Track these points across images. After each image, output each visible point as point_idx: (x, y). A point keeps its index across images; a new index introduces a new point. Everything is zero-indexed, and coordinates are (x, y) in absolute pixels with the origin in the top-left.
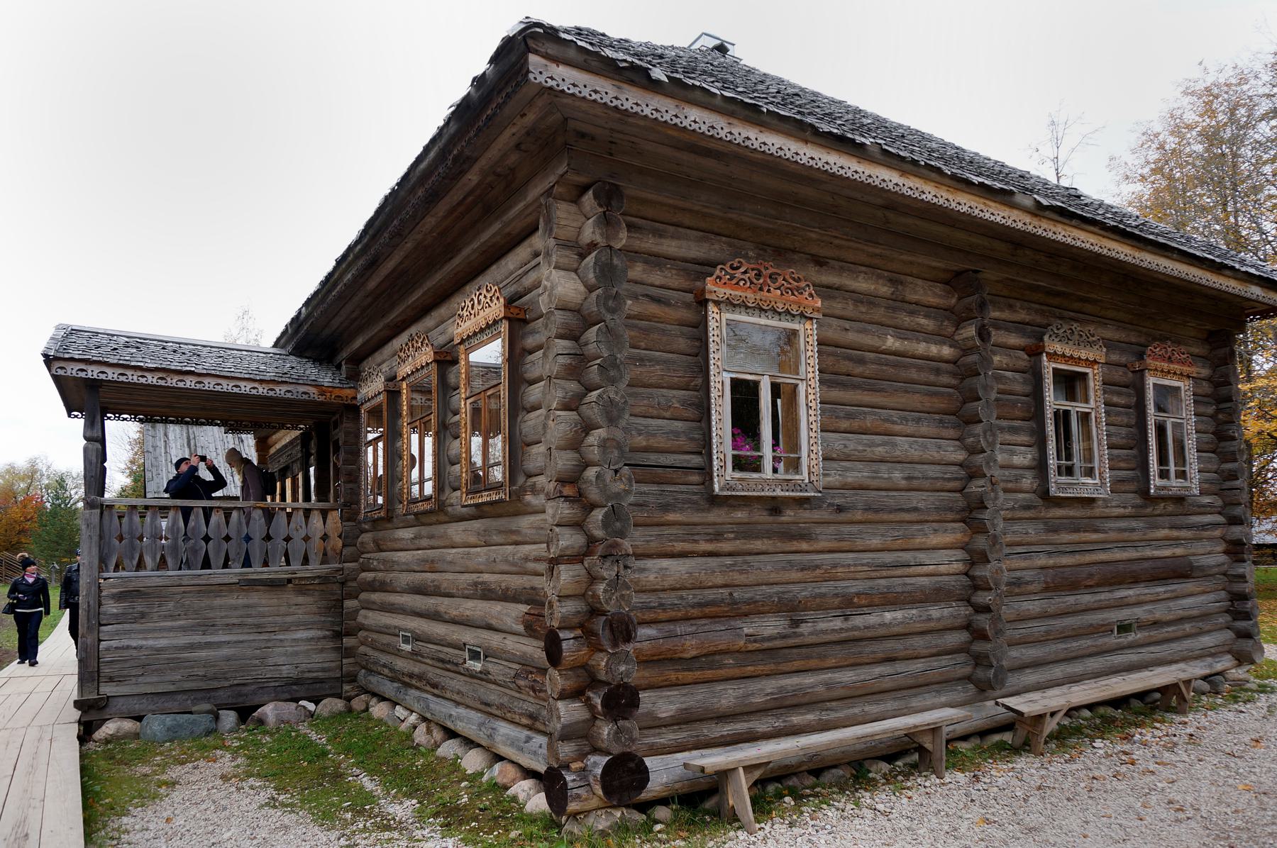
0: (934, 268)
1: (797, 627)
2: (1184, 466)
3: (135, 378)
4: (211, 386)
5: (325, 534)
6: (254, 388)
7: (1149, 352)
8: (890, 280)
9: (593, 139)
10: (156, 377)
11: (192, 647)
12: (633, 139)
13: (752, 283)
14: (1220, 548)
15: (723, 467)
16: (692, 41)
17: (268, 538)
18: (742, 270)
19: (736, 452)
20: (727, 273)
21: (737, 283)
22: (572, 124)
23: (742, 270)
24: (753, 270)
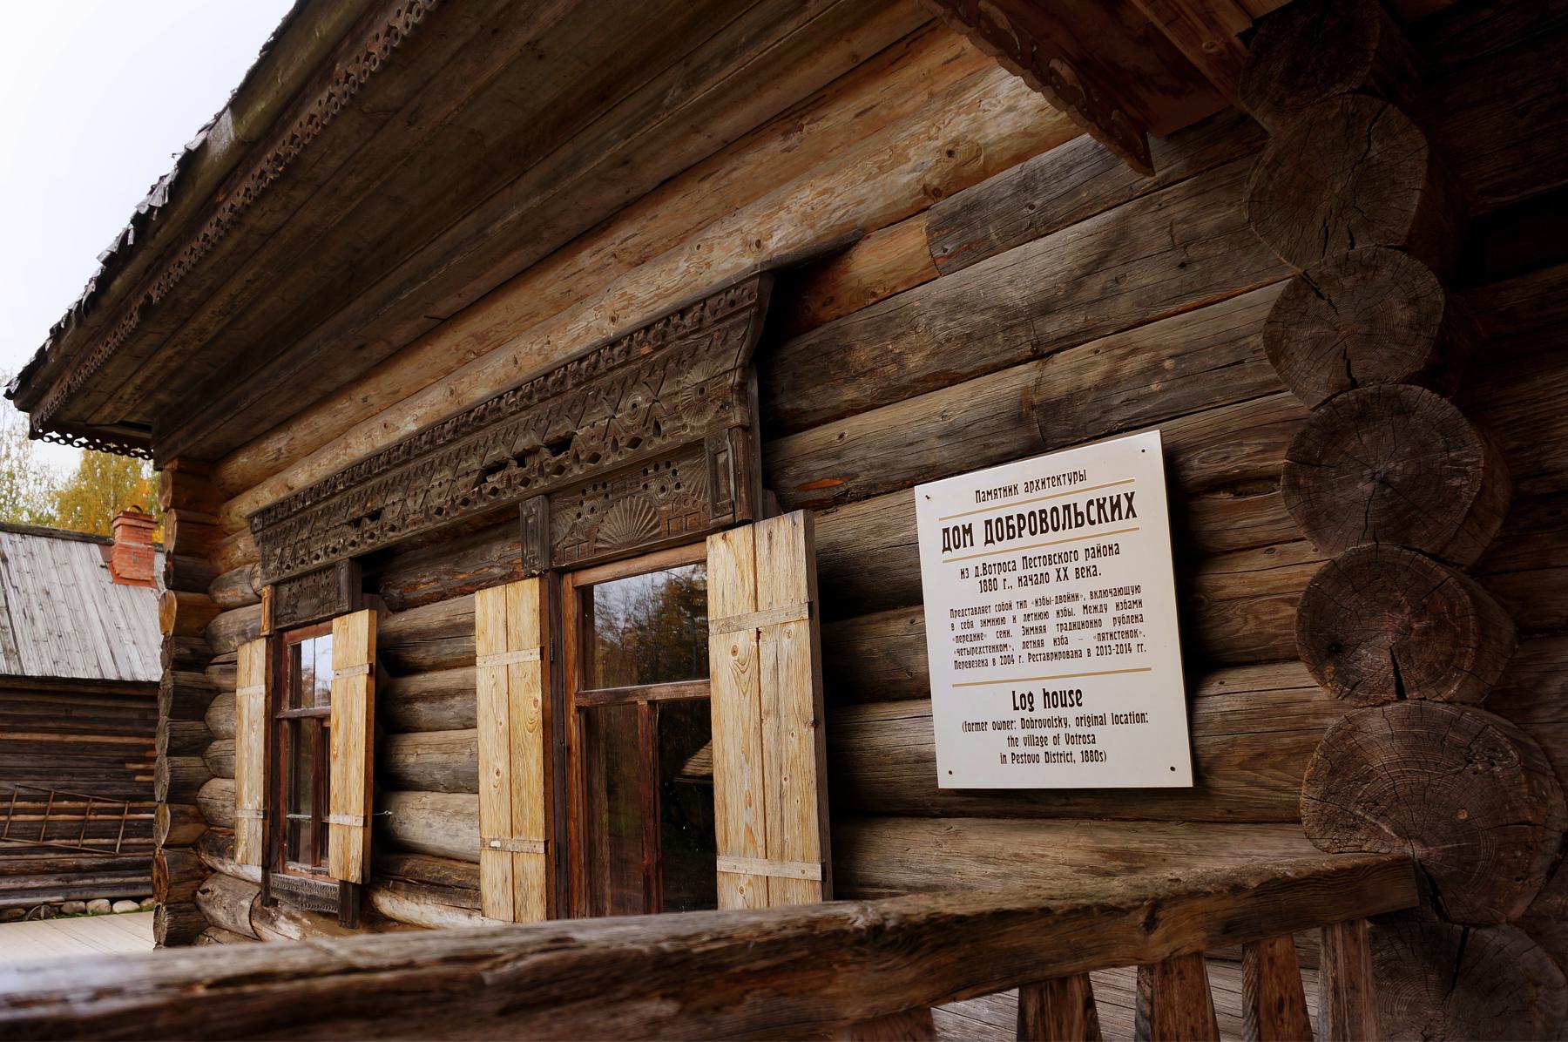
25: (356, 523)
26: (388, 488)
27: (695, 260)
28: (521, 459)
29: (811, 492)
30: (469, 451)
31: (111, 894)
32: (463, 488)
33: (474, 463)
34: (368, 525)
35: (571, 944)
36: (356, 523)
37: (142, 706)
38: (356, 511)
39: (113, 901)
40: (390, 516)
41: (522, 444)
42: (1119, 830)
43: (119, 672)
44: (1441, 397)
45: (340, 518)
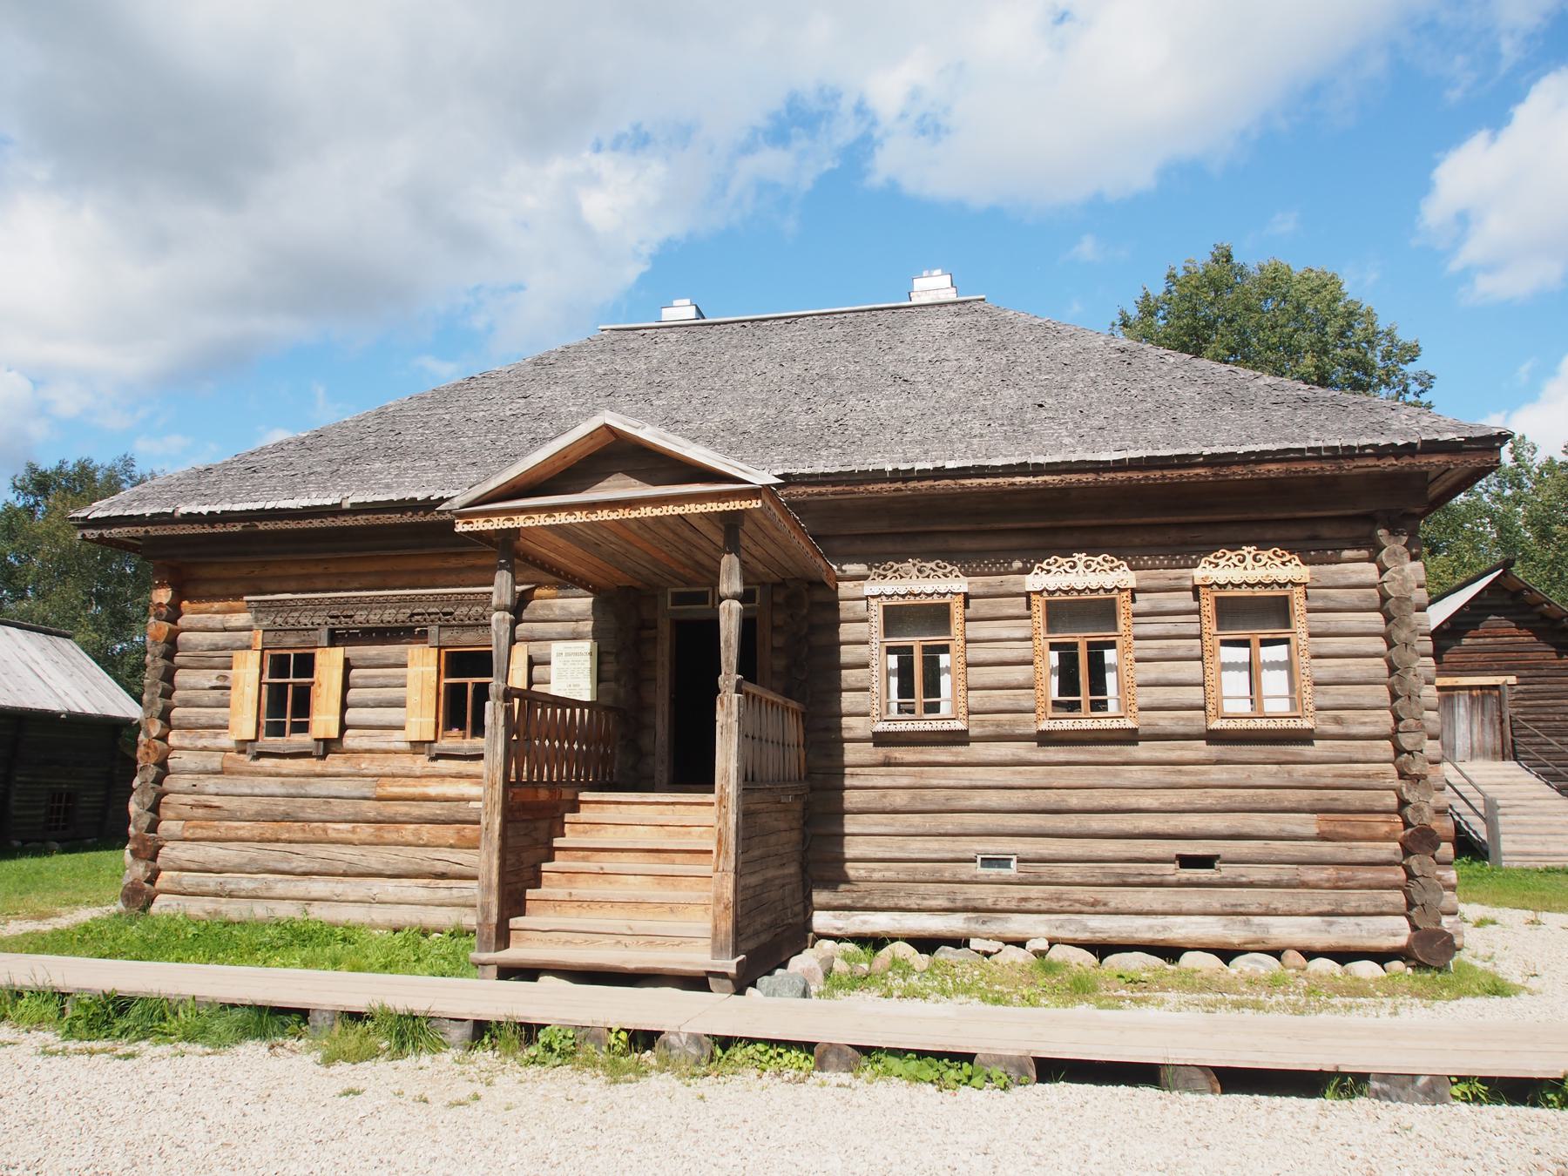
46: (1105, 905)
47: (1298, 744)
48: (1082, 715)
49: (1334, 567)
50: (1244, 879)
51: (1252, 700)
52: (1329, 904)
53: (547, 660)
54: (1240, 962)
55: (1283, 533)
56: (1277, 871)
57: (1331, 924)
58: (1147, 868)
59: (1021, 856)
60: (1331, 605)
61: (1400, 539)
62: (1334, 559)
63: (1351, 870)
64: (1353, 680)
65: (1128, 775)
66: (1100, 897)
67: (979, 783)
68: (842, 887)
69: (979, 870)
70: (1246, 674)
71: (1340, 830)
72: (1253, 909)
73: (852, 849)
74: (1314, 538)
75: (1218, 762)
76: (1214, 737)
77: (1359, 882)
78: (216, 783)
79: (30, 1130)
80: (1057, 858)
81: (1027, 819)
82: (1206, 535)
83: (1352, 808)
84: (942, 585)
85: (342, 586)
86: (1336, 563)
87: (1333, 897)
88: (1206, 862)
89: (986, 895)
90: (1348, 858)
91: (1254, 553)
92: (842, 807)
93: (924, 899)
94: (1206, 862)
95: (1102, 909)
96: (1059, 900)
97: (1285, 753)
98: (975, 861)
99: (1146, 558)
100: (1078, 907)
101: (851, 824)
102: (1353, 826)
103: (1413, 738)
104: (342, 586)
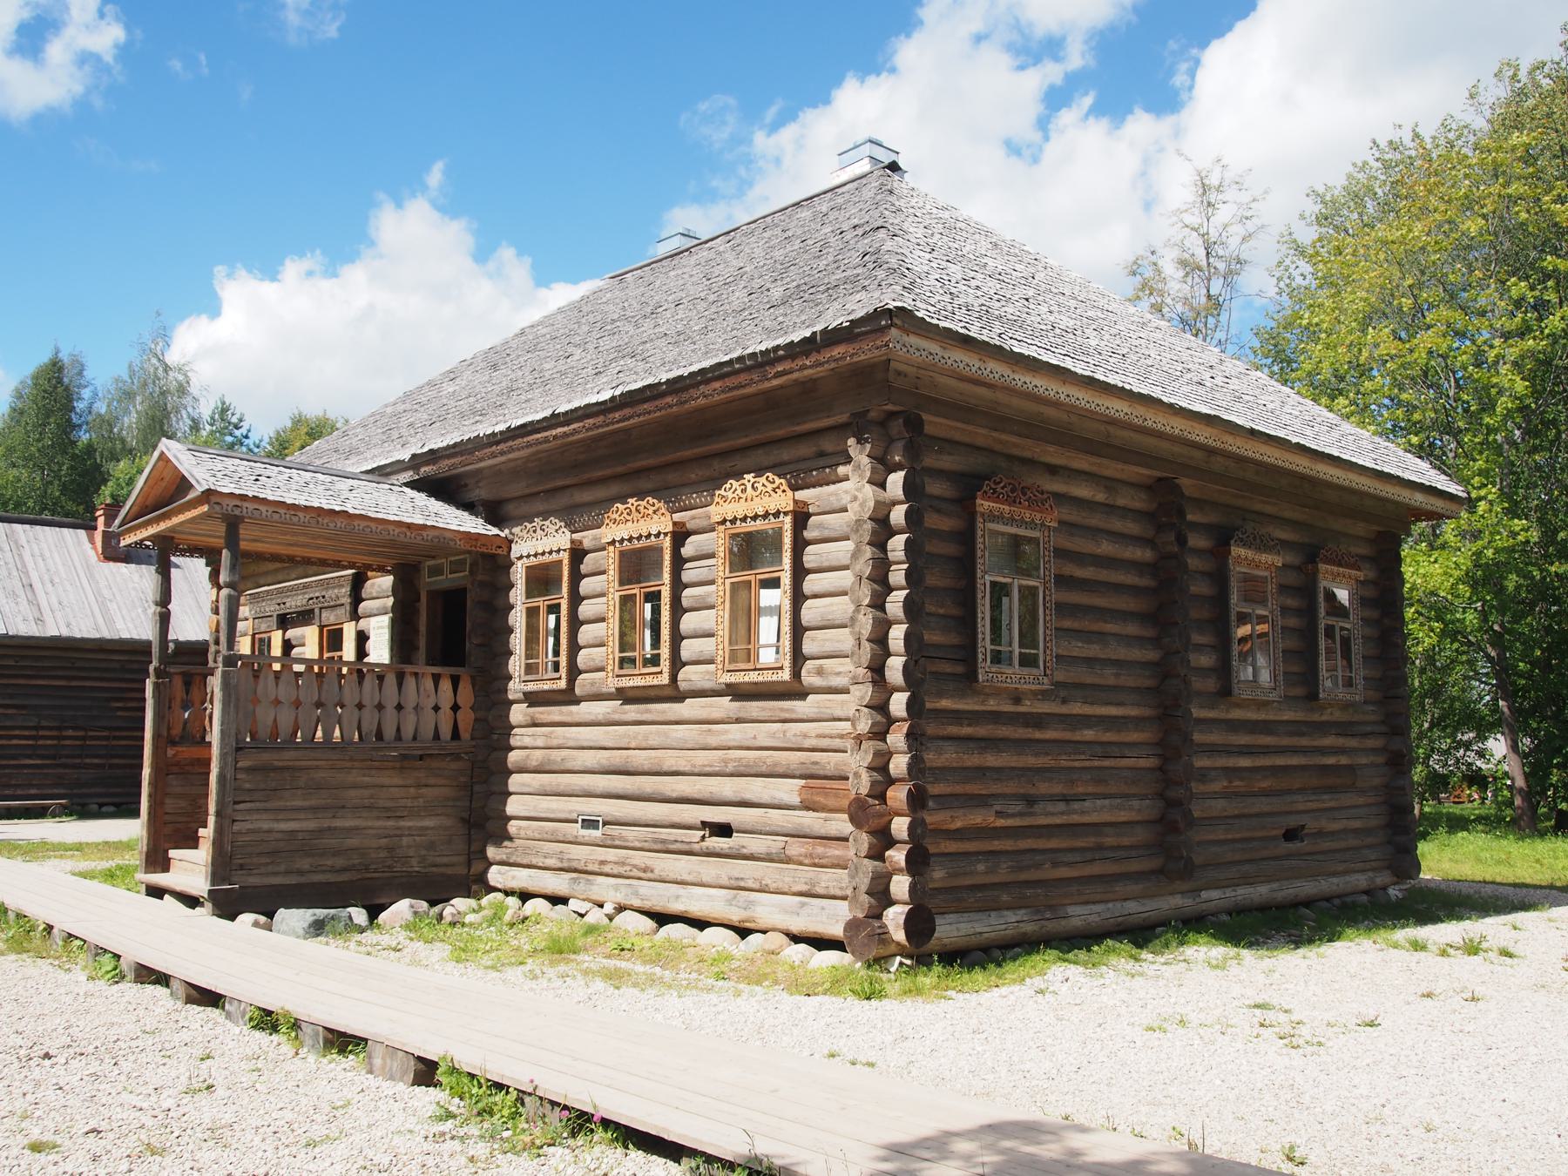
0: (1142, 474)
1: (1032, 807)
2: (1351, 672)
3: (288, 516)
4: (229, 509)
5: (360, 709)
6: (368, 526)
7: (1321, 556)
8: (1106, 487)
9: (906, 376)
10: (308, 517)
11: (320, 832)
12: (931, 374)
13: (1008, 496)
14: (1380, 759)
15: (985, 660)
16: (845, 149)
17: (399, 707)
18: (1002, 485)
19: (993, 647)
20: (991, 488)
21: (998, 497)
22: (892, 364)
23: (1002, 485)
24: (1010, 484)
25: (279, 604)
26: (288, 597)
27: (1338, 995)
28: (317, 598)
29: (1133, 685)
30: (305, 593)
31: (101, 800)
32: (304, 602)
33: (307, 596)
34: (282, 606)
35: (407, 476)
36: (279, 604)
37: (122, 658)
38: (279, 601)
39: (101, 805)
40: (288, 605)
41: (317, 595)
42: (778, 826)
43: (816, 596)
44: (760, 611)
45: (274, 602)
46: (652, 871)
47: (796, 699)
48: (539, 677)
49: (832, 488)
50: (745, 851)
51: (778, 648)
52: (806, 883)
53: (302, 642)
54: (531, 903)
55: (760, 457)
56: (770, 843)
57: (803, 905)
58: (685, 835)
59: (607, 819)
60: (826, 534)
61: (865, 448)
62: (833, 478)
63: (825, 846)
64: (837, 622)
65: (674, 735)
66: (649, 863)
67: (585, 744)
68: (506, 843)
69: (576, 830)
70: (776, 618)
71: (817, 798)
72: (750, 884)
73: (513, 806)
74: (822, 454)
75: (738, 721)
76: (738, 693)
77: (830, 860)
78: (1481, 754)
79: (552, 1138)
80: (623, 821)
81: (609, 780)
82: (717, 466)
83: (665, 768)
84: (644, 527)
85: (287, 578)
86: (834, 483)
87: (810, 875)
88: (724, 830)
89: (579, 854)
90: (823, 832)
91: (752, 480)
92: (507, 768)
93: (545, 857)
94: (724, 830)
95: (649, 875)
96: (623, 864)
97: (782, 710)
98: (577, 822)
99: (694, 495)
100: (636, 873)
101: (515, 782)
102: (826, 795)
103: (860, 690)
104: (262, 582)
